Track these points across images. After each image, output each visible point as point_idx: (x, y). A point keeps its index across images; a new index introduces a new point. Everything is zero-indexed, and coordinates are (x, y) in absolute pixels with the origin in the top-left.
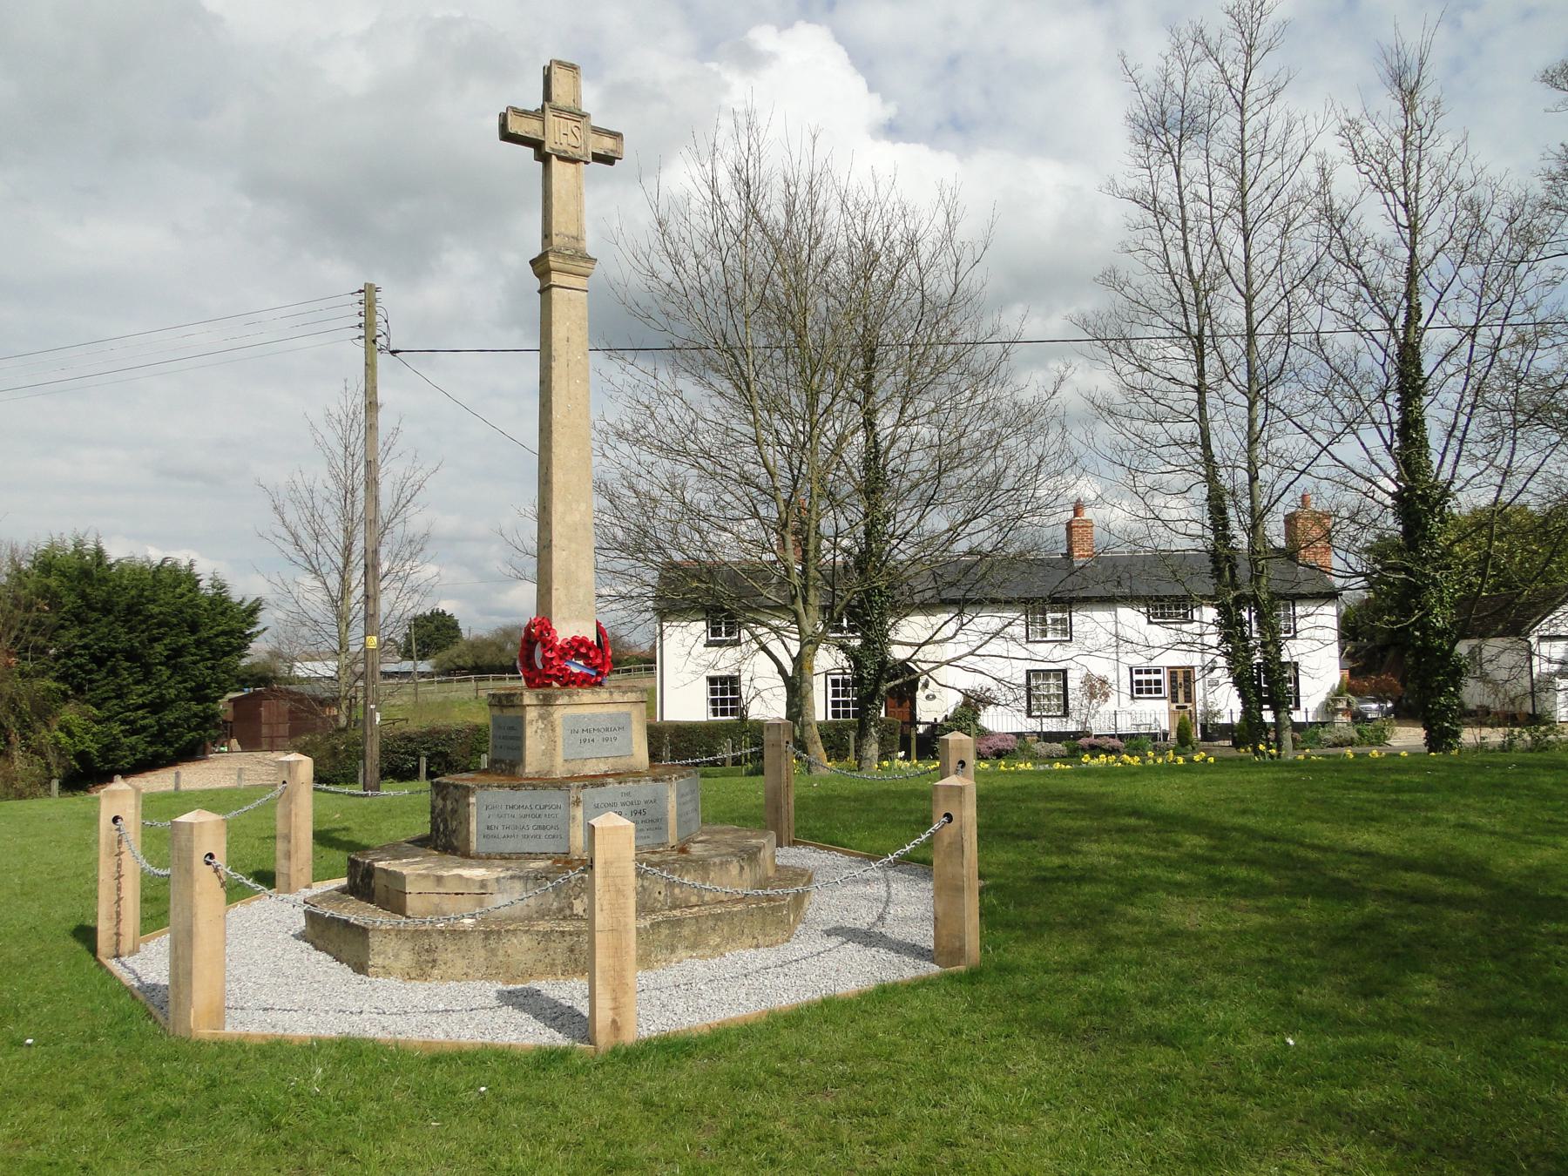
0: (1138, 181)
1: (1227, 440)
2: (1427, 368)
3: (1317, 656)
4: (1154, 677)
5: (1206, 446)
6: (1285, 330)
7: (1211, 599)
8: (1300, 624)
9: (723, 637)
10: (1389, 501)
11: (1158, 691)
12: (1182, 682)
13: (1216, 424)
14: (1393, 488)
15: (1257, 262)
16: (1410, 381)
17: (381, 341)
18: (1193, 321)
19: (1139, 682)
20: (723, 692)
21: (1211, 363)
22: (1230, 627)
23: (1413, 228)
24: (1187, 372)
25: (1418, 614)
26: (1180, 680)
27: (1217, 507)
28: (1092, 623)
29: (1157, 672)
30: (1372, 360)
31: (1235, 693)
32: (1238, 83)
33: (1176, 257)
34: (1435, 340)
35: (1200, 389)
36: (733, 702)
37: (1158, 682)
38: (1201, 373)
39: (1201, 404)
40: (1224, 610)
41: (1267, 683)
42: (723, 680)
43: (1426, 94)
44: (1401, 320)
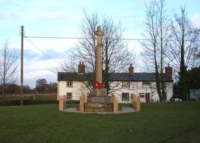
0: (147, 21)
1: (158, 60)
2: (185, 50)
3: (170, 94)
4: (143, 94)
5: (155, 59)
6: (166, 45)
7: (155, 81)
8: (167, 85)
9: (70, 86)
10: (179, 68)
11: (144, 97)
12: (148, 95)
13: (157, 57)
14: (180, 66)
15: (163, 34)
16: (183, 52)
17: (24, 35)
18: (154, 42)
19: (141, 95)
20: (69, 95)
21: (156, 48)
22: (158, 85)
23: (183, 30)
24: (153, 49)
25: (27, 90)
26: (147, 95)
27: (156, 67)
28: (133, 85)
29: (144, 94)
30: (178, 49)
31: (158, 95)
32: (161, 10)
33: (152, 33)
34: (186, 46)
35: (155, 51)
36: (71, 97)
37: (144, 95)
38: (155, 50)
39: (155, 53)
40: (157, 83)
41: (163, 96)
42: (69, 93)
43: (185, 12)
44: (181, 43)
